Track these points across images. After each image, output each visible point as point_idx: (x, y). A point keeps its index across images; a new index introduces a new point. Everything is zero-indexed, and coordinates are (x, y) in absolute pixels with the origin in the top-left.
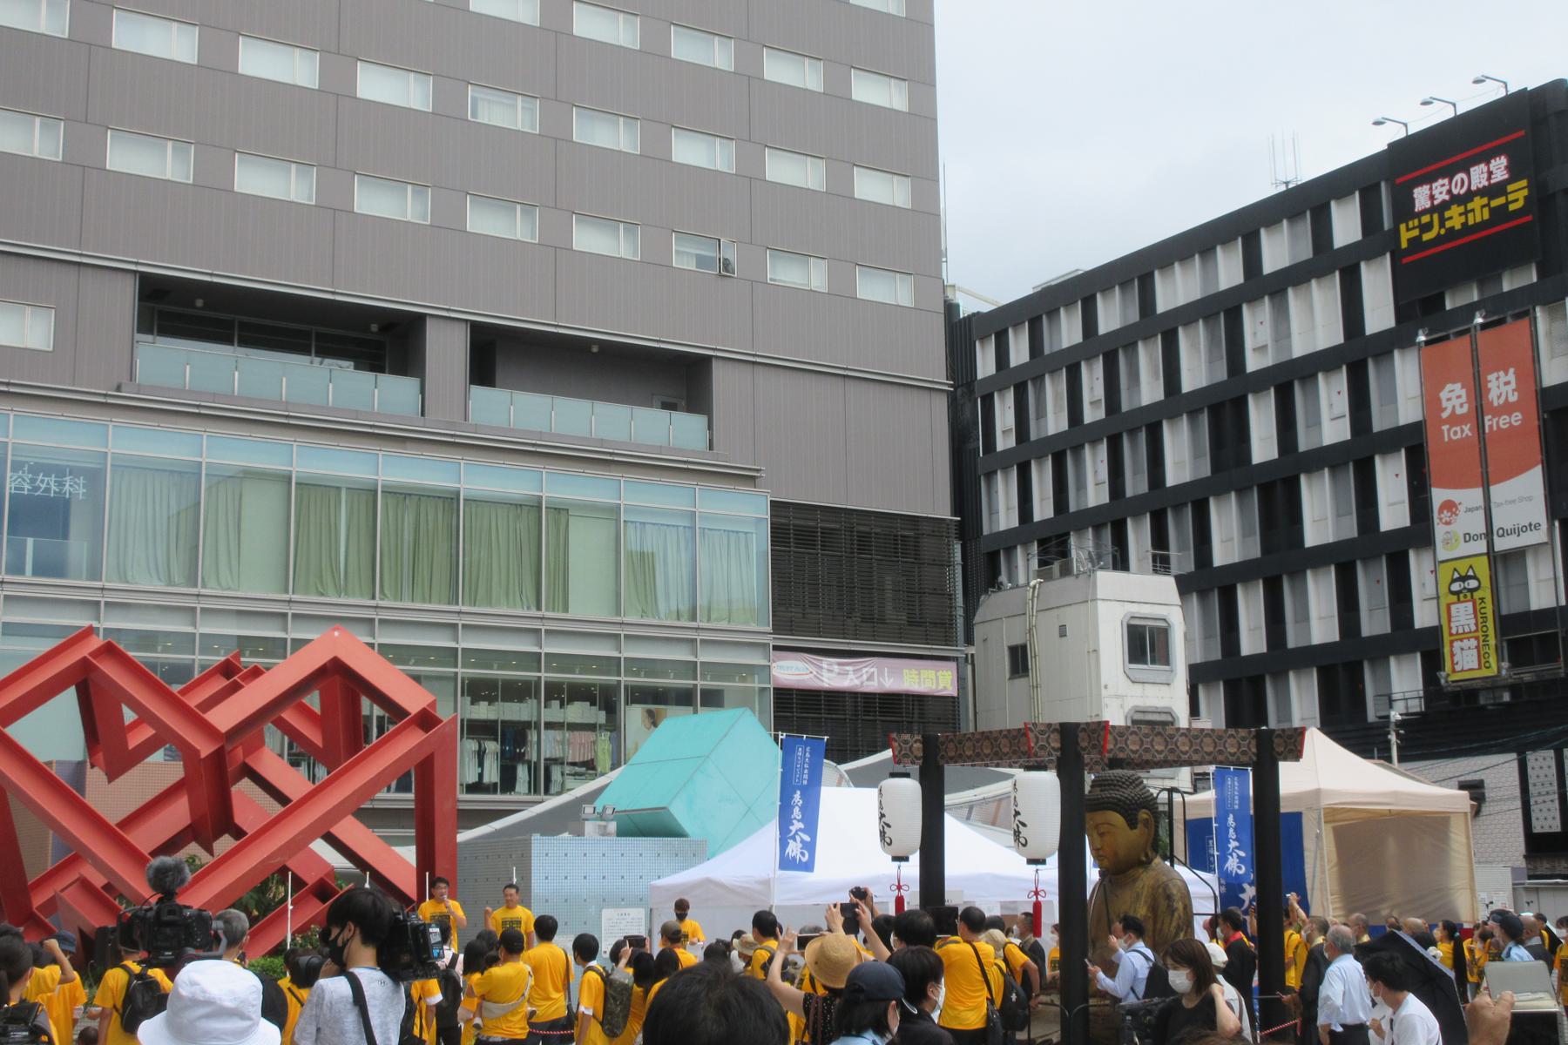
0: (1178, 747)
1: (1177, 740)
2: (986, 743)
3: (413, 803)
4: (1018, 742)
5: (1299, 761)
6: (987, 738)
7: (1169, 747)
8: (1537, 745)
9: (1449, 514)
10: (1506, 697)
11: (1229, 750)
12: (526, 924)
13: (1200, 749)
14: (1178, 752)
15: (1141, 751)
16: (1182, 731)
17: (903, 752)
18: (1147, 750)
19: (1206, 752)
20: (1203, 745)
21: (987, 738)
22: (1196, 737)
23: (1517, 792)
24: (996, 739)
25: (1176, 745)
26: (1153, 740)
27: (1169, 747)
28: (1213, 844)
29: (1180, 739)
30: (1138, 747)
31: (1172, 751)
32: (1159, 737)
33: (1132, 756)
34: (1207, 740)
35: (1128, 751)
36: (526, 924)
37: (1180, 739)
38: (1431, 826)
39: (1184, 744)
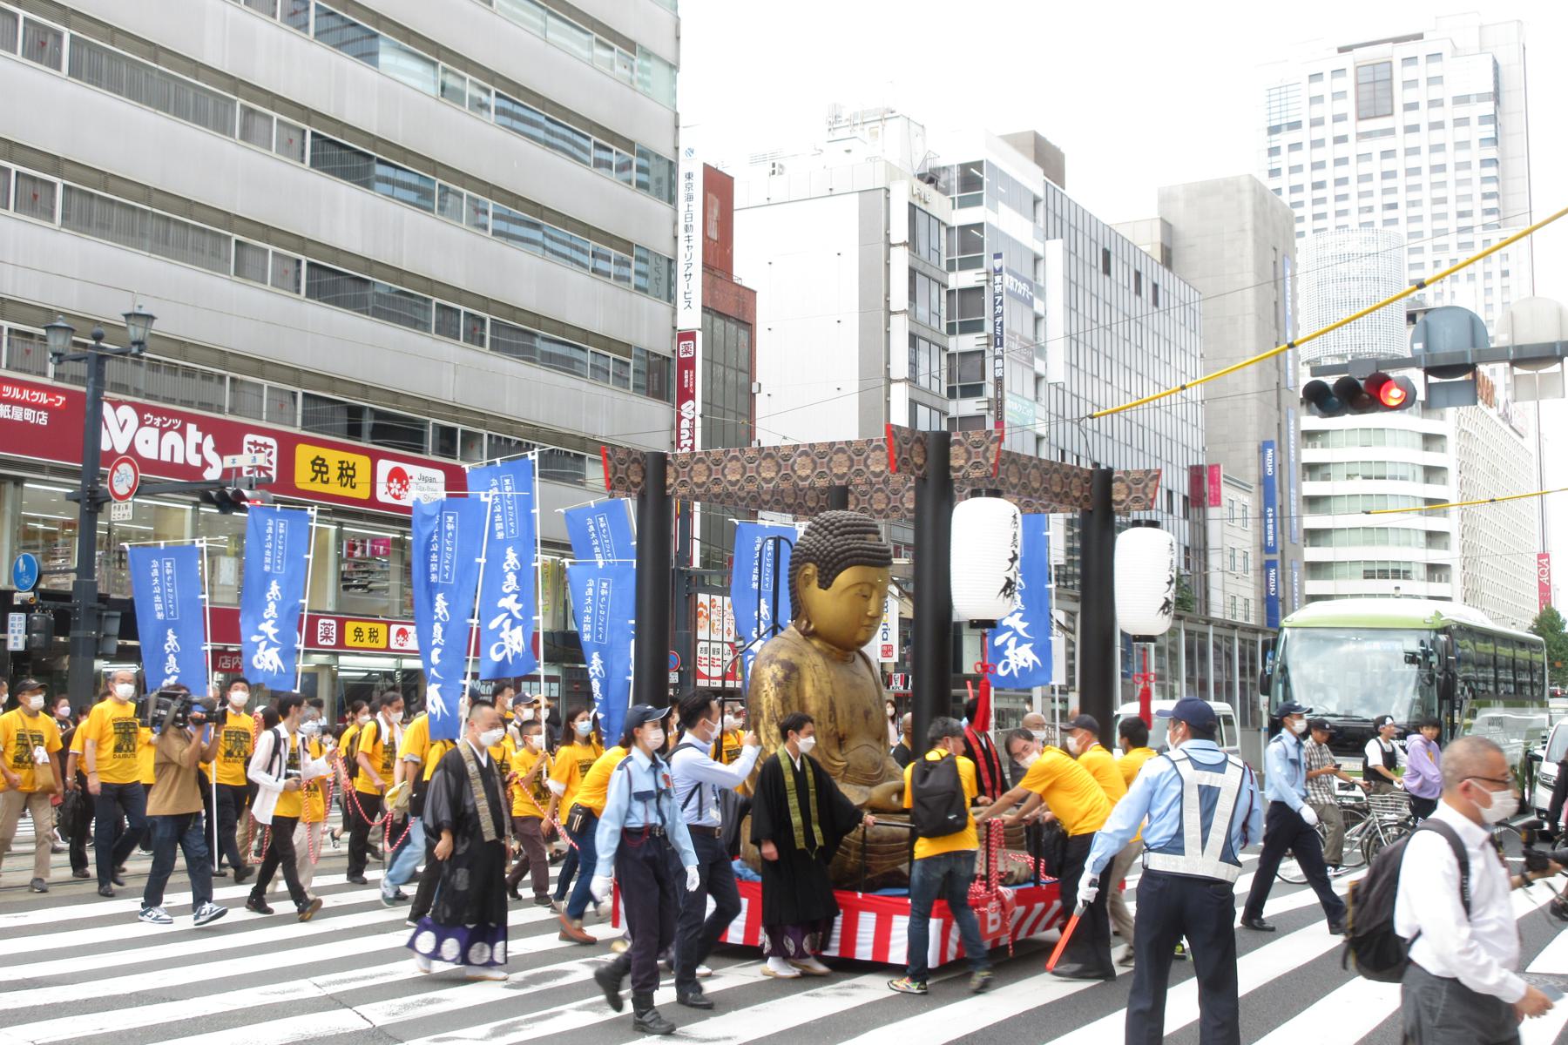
0: (795, 472)
1: (795, 462)
2: (1012, 468)
3: (169, 459)
4: (744, 473)
5: (731, 179)
6: (1014, 461)
7: (783, 472)
8: (165, 463)
9: (399, 486)
10: (492, 925)
11: (872, 468)
12: (1109, 875)
13: (983, 461)
14: (795, 478)
15: (742, 482)
16: (837, 446)
17: (1141, 486)
18: (751, 480)
19: (836, 475)
20: (988, 454)
21: (1014, 461)
22: (822, 455)
23: (369, 480)
24: (1025, 467)
25: (793, 470)
26: (628, 468)
27: (783, 472)
28: (203, 565)
29: (799, 460)
30: (738, 477)
31: (786, 477)
32: (769, 460)
33: (801, 484)
34: (841, 457)
35: (795, 478)
36: (1109, 875)
37: (799, 460)
38: (54, 533)
39: (804, 467)
